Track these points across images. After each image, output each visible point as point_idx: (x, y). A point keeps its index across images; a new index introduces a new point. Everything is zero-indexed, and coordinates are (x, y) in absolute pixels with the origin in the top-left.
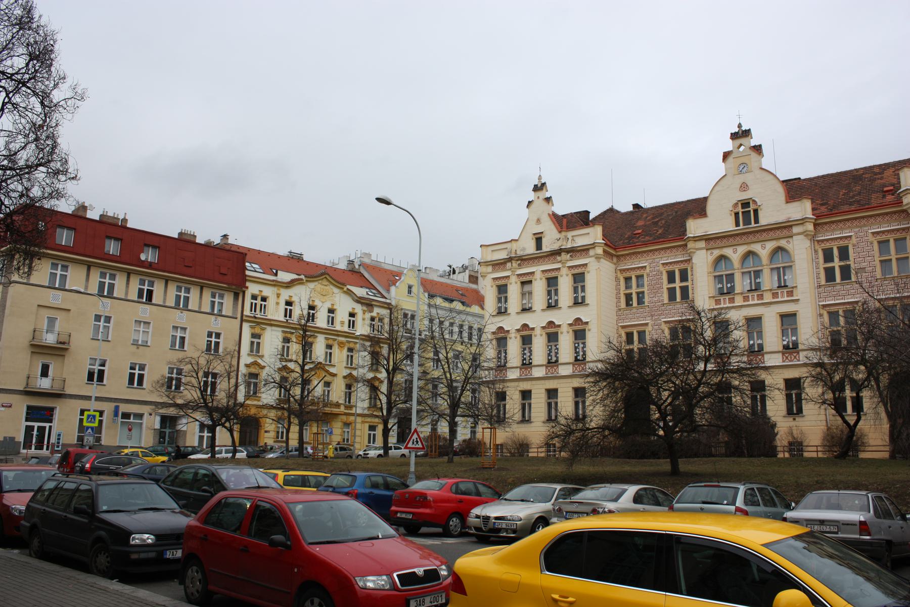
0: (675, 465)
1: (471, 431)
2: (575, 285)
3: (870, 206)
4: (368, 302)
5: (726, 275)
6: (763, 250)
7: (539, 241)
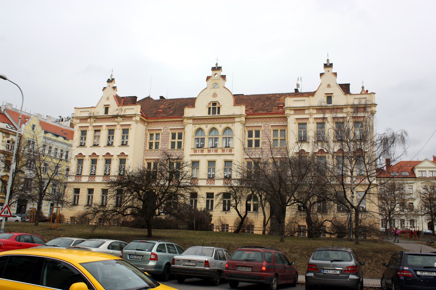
0: (150, 232)
2: (123, 135)
3: (272, 113)
4: (7, 132)
5: (201, 138)
6: (220, 128)
7: (107, 109)
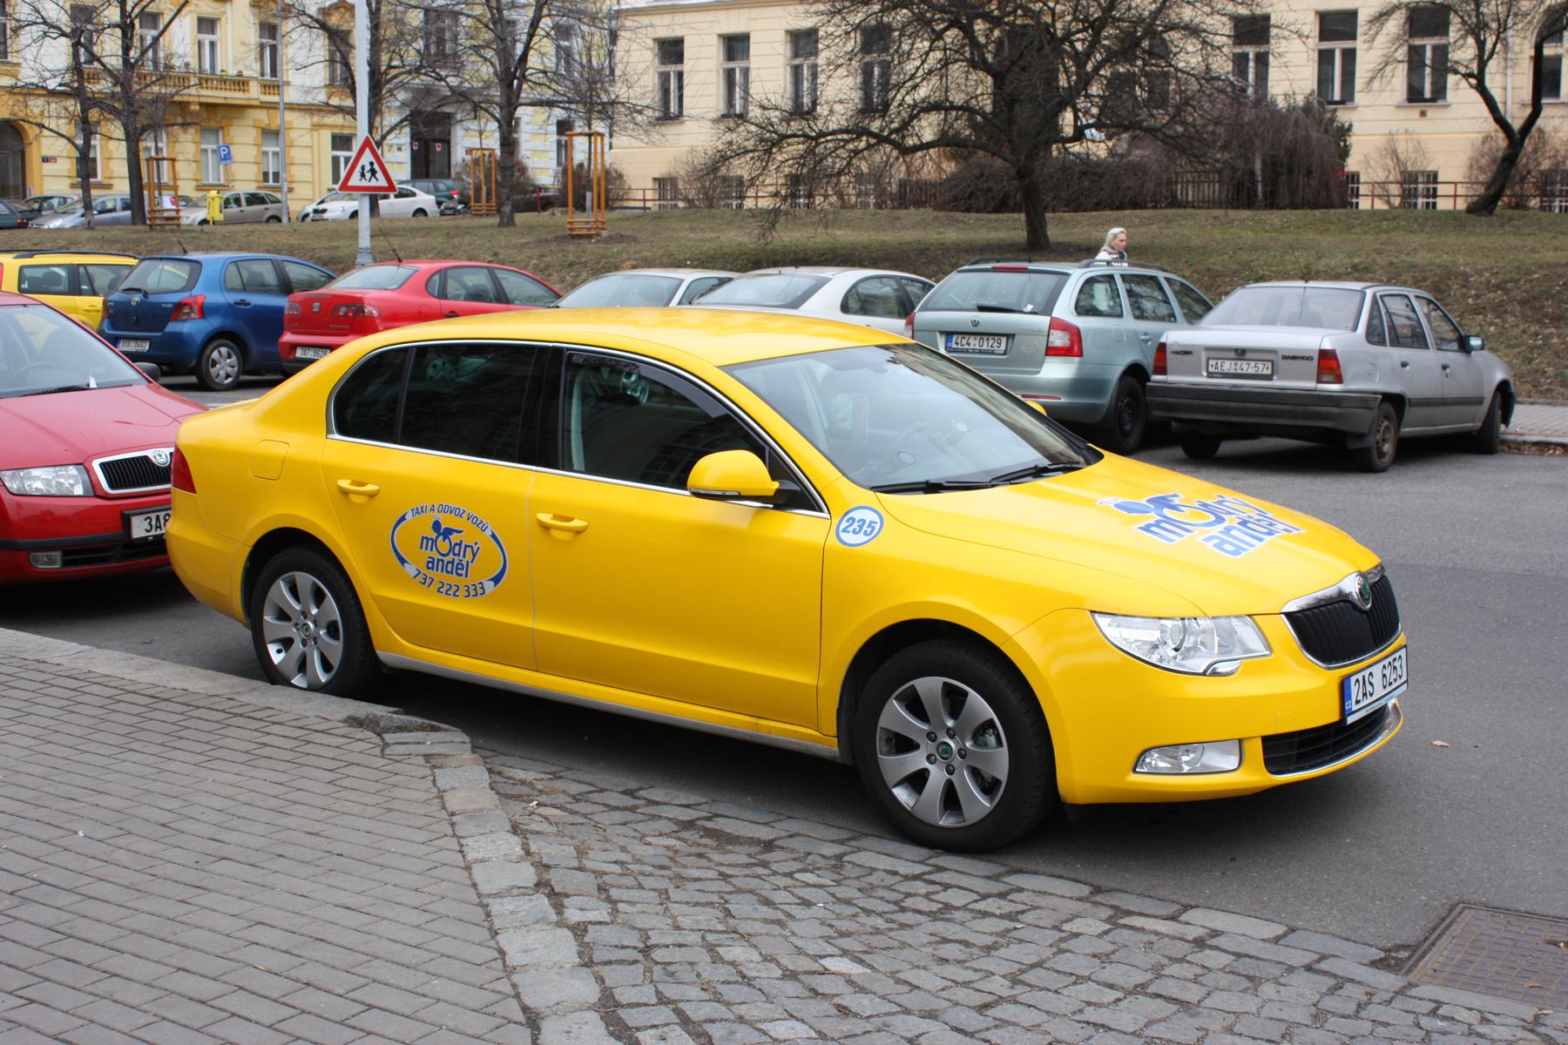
1: (559, 143)
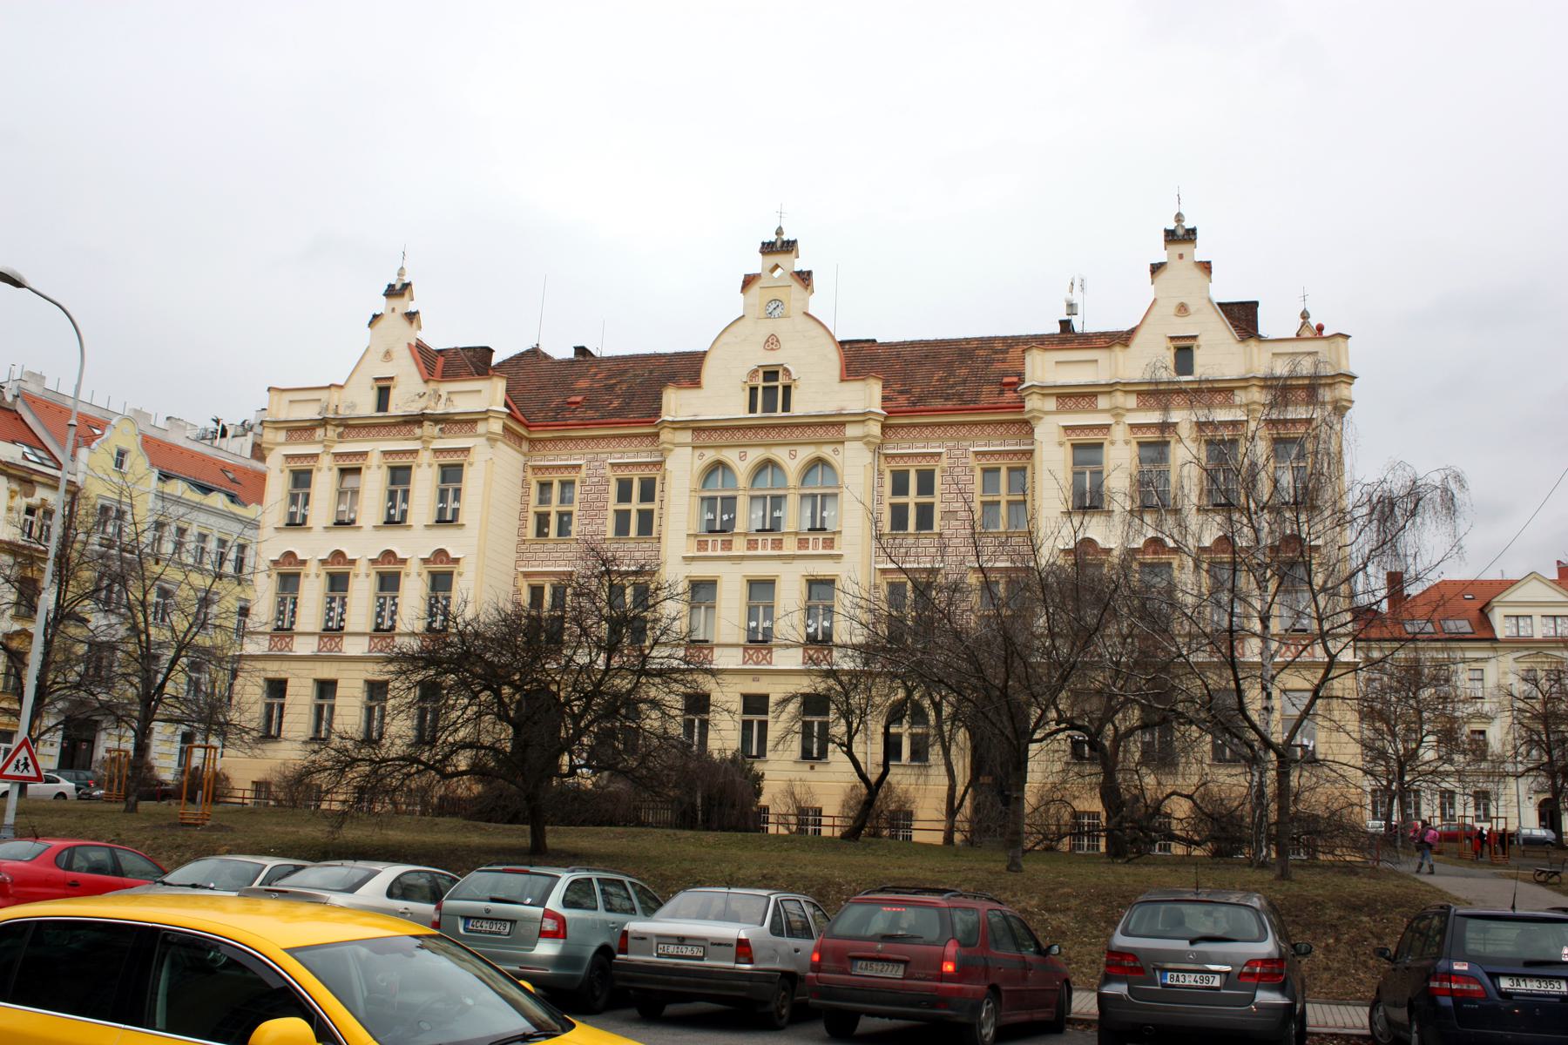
0: (538, 836)
2: (444, 486)
3: (977, 406)
4: (24, 475)
5: (723, 498)
6: (792, 460)
7: (383, 394)
